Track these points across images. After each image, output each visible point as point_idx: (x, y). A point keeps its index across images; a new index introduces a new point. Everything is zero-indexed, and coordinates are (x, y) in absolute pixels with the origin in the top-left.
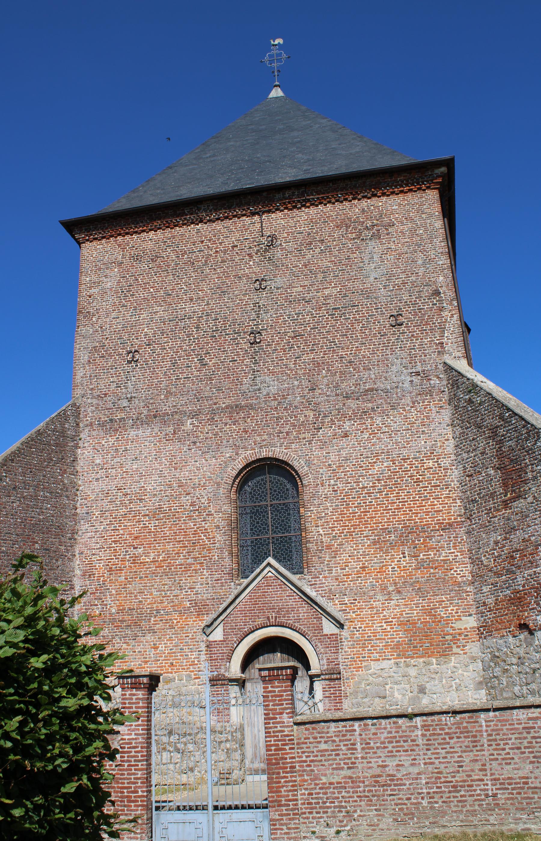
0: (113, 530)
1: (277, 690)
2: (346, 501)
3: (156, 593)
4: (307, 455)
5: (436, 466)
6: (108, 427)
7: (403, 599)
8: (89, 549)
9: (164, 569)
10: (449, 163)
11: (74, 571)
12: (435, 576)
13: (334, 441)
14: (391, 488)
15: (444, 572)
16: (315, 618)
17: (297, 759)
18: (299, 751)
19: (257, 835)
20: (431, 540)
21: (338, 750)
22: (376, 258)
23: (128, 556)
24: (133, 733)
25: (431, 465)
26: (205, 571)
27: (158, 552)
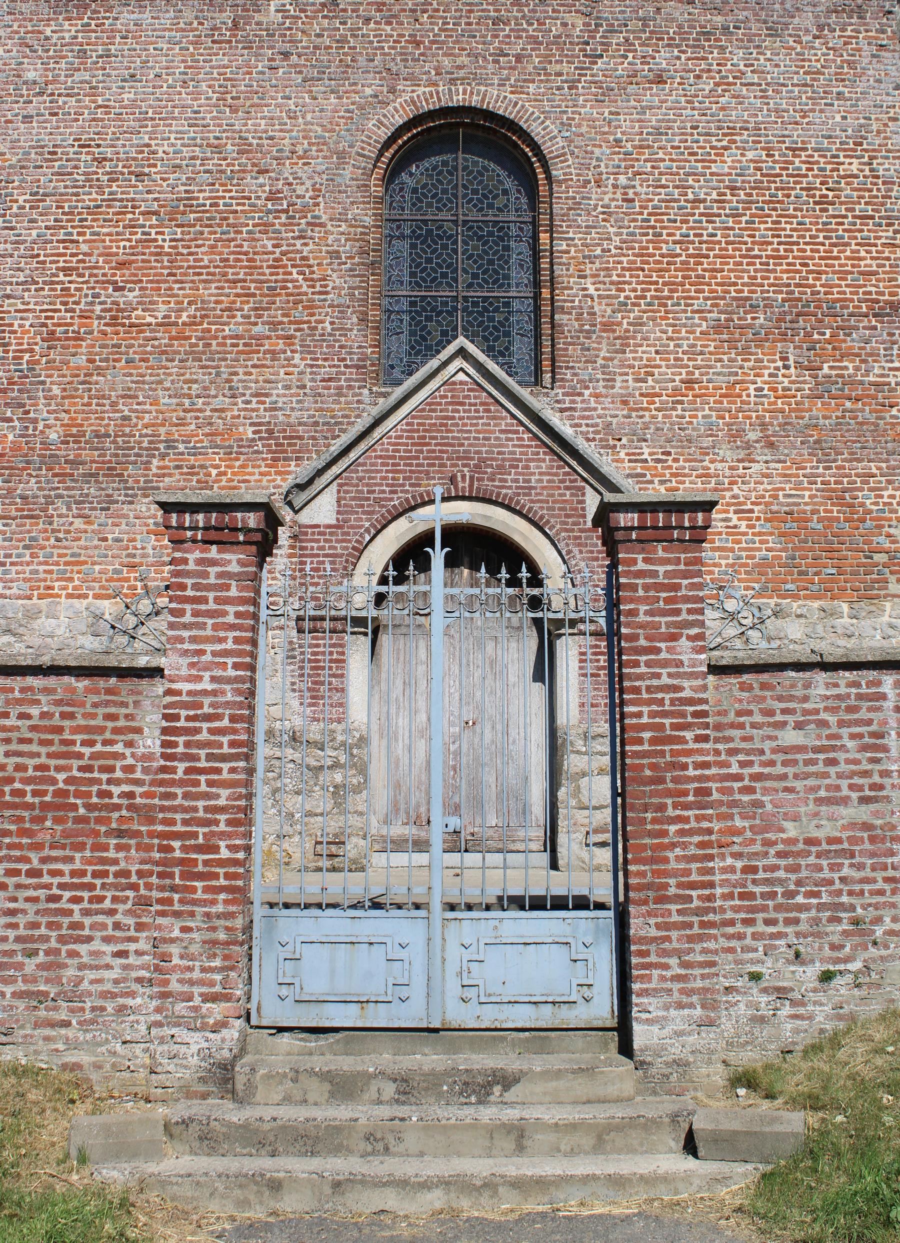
0: (64, 241)
1: (661, 569)
2: (654, 227)
3: (166, 400)
4: (565, 112)
5: (867, 173)
7: (779, 461)
9: (192, 345)
12: (856, 417)
13: (631, 89)
14: (762, 209)
15: (876, 411)
16: (567, 488)
17: (714, 771)
18: (720, 746)
19: (575, 982)
20: (849, 335)
21: (833, 748)
23: (98, 308)
24: (207, 675)
25: (854, 168)
26: (297, 356)
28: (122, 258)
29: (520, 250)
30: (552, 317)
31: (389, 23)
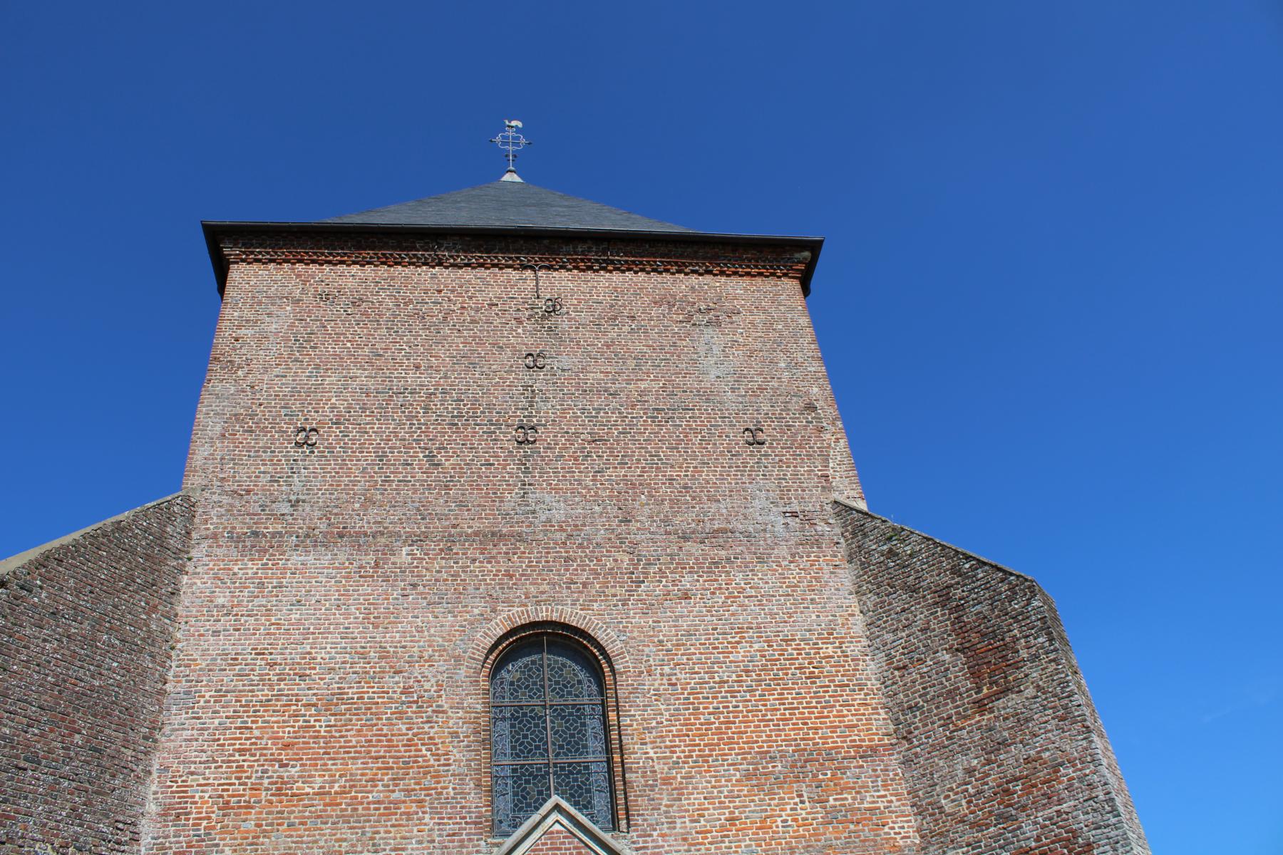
0: (240, 728)
6: (248, 544)
8: (184, 763)
9: (342, 810)
10: (820, 243)
11: (143, 805)
22: (716, 350)
23: (266, 781)
25: (830, 651)
26: (427, 816)
27: (331, 776)
28: (287, 740)
29: (594, 724)
30: (624, 776)
31: (489, 562)
